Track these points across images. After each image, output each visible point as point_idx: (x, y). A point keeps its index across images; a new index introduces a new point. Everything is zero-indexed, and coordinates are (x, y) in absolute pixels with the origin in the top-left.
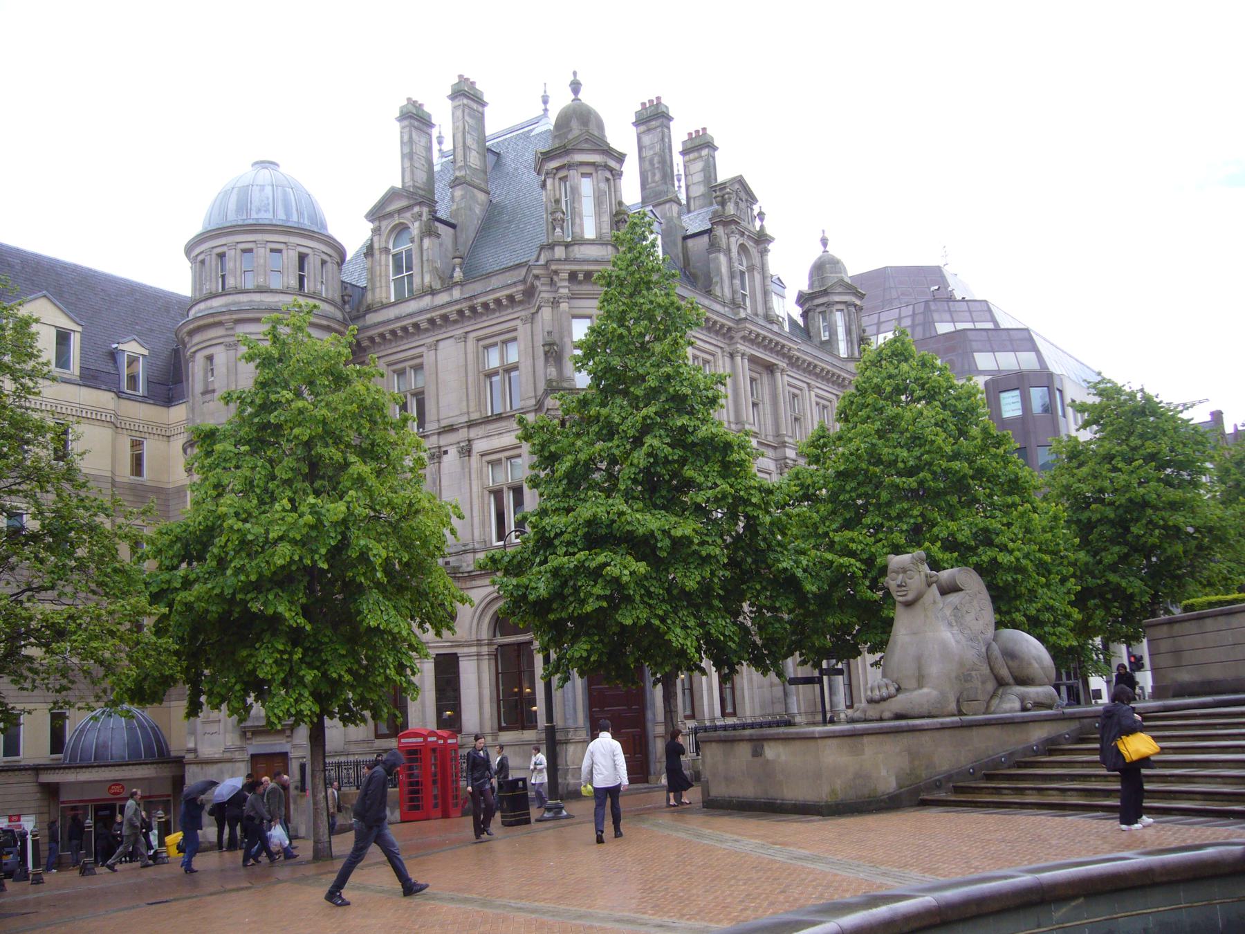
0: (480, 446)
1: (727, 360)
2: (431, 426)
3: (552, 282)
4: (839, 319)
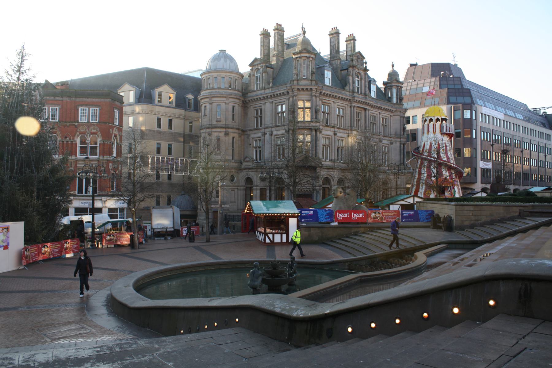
0: (274, 133)
1: (349, 108)
2: (263, 126)
3: (293, 91)
4: (394, 91)
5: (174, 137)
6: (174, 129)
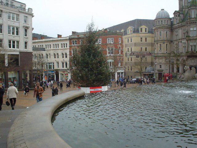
0: (182, 42)
5: (148, 44)
6: (148, 41)
